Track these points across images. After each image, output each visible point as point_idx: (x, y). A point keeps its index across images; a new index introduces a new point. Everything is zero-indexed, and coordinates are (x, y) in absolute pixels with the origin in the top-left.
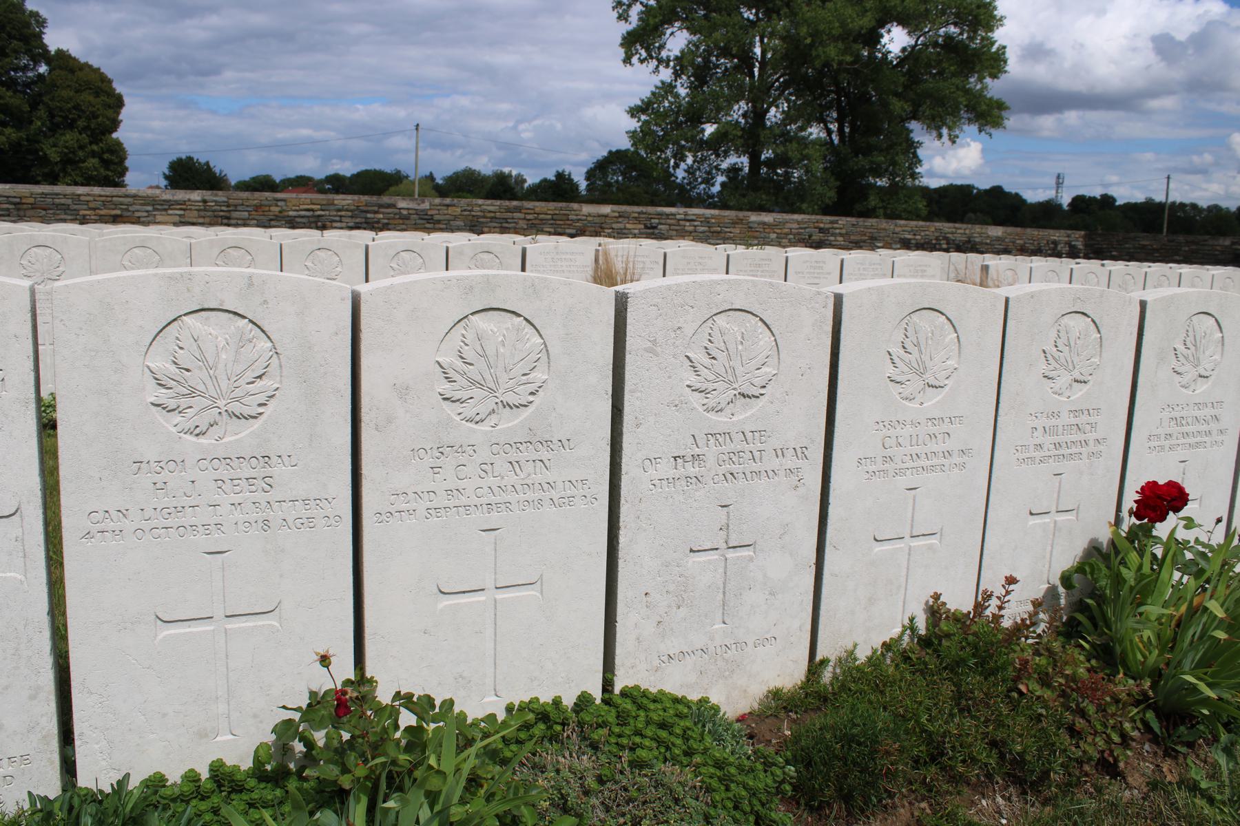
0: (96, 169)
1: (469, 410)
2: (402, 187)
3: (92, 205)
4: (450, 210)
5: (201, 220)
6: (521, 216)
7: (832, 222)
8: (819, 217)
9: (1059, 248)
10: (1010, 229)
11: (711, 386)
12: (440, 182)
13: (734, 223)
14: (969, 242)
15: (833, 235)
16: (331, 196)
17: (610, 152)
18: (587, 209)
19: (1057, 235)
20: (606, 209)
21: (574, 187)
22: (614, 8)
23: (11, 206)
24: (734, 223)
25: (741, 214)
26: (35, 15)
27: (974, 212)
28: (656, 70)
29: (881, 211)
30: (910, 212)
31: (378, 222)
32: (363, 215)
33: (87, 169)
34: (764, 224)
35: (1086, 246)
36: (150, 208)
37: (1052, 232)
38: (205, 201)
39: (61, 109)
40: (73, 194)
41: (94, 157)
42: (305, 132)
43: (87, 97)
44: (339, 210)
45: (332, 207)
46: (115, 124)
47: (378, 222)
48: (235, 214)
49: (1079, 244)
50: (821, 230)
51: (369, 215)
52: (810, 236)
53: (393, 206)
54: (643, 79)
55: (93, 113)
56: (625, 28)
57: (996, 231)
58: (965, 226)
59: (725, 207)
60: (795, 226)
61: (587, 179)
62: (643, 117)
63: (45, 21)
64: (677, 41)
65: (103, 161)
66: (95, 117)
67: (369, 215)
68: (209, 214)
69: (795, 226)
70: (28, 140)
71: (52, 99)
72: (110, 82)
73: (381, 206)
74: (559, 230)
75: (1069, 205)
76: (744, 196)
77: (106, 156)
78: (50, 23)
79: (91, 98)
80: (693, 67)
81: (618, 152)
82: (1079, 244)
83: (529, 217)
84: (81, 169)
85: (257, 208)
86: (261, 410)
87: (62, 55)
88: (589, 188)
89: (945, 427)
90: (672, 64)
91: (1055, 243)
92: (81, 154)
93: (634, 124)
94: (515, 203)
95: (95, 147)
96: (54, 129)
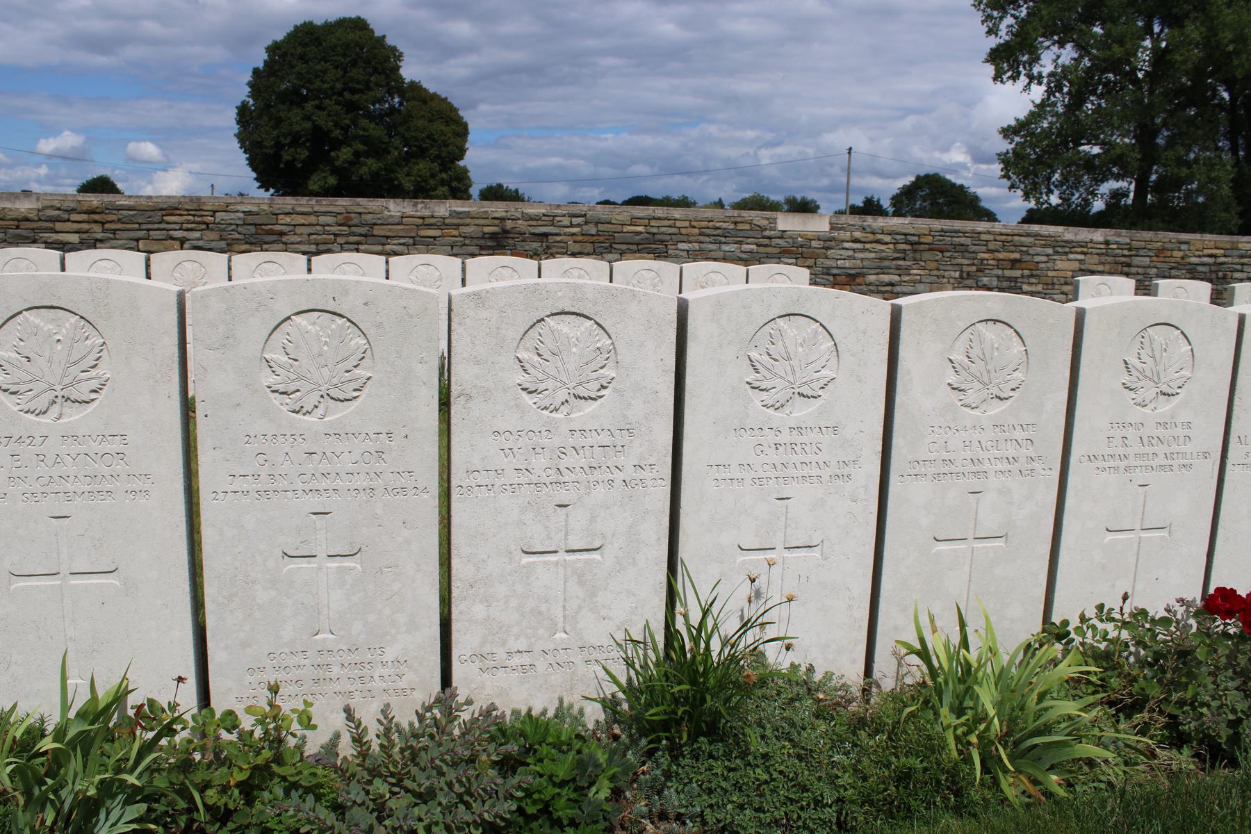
3: (992, 246)
5: (1100, 268)
16: (1235, 238)
17: (918, 178)
22: (983, 22)
23: (908, 247)
26: (394, 49)
28: (1027, 88)
36: (1050, 251)
38: (1107, 243)
39: (416, 139)
40: (974, 232)
41: (443, 185)
42: (554, 160)
43: (439, 126)
45: (1236, 253)
46: (461, 152)
48: (1136, 261)
54: (1014, 100)
55: (444, 142)
56: (993, 42)
57: (395, 208)
62: (1017, 139)
63: (401, 55)
64: (1055, 57)
66: (446, 144)
68: (1110, 259)
70: (385, 169)
71: (408, 129)
72: (456, 110)
74: (322, 247)
77: (454, 184)
78: (405, 58)
79: (443, 128)
80: (1076, 85)
81: (927, 176)
85: (1160, 252)
86: (93, 396)
87: (415, 87)
90: (1045, 80)
92: (432, 182)
93: (1005, 146)
95: (444, 176)
96: (408, 157)
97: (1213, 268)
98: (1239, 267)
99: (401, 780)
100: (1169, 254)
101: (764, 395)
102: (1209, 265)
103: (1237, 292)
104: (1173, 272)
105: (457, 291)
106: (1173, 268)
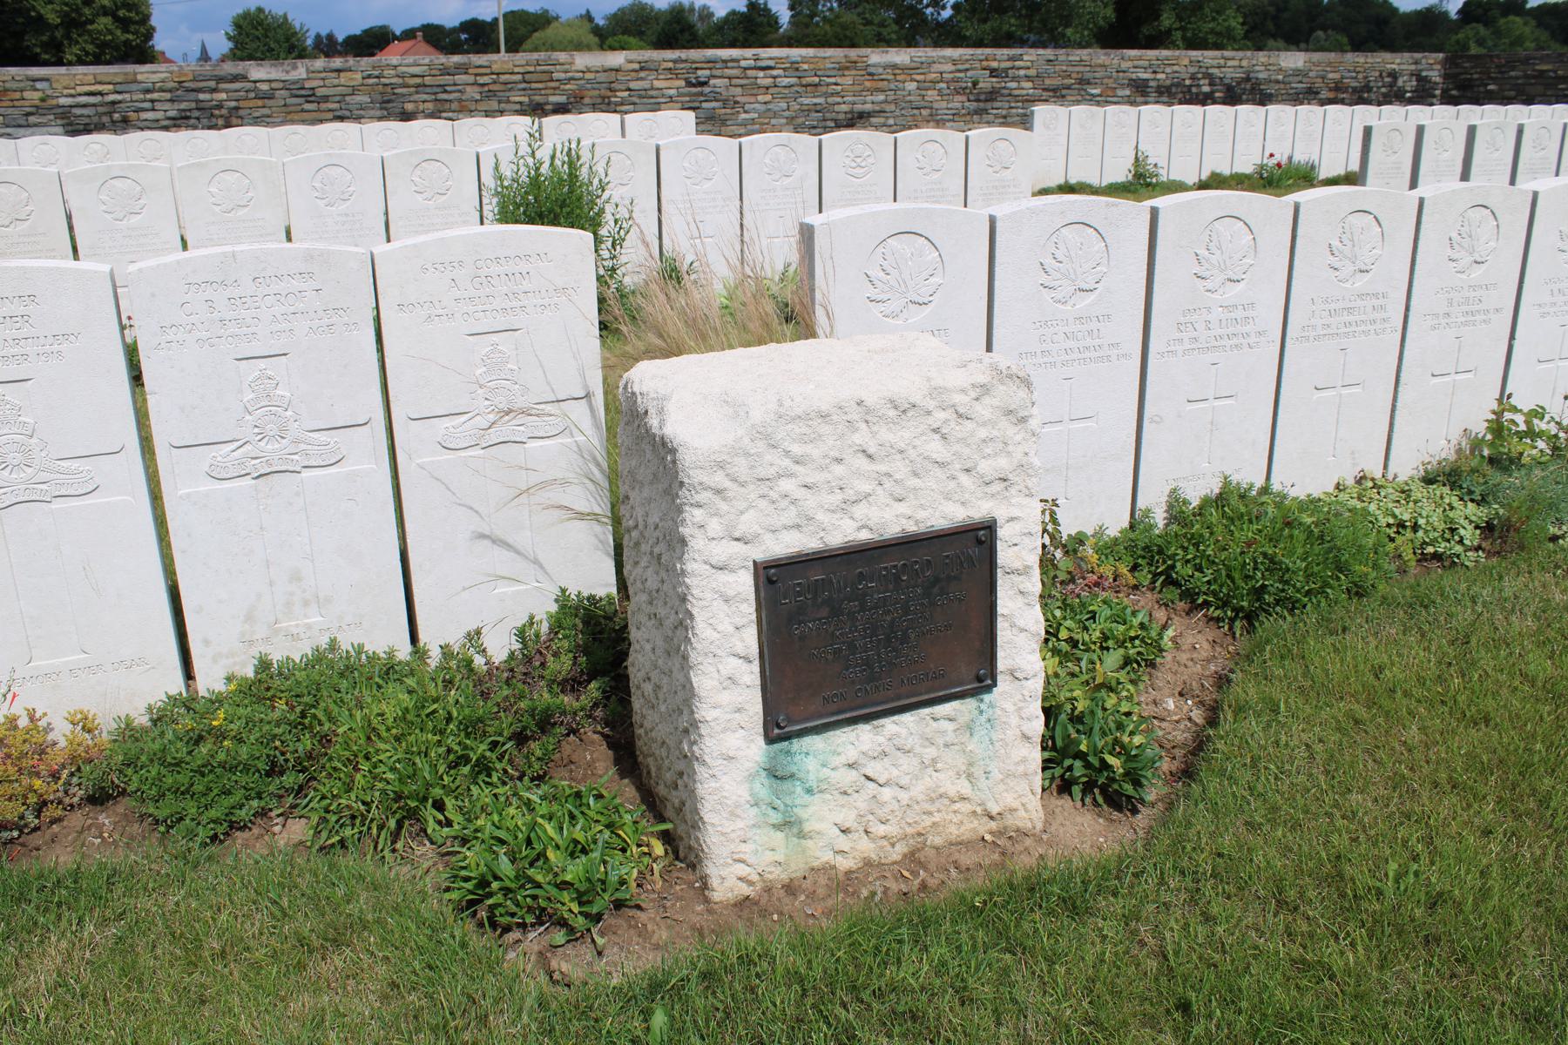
0: (110, 32)
1: (1058, 295)
2: (549, 32)
4: (344, 78)
6: (471, 79)
7: (1012, 59)
8: (988, 51)
9: (1400, 83)
10: (1317, 56)
11: (1057, 283)
12: (601, 23)
13: (842, 69)
14: (1248, 79)
15: (1014, 79)
18: (582, 60)
19: (1399, 62)
20: (617, 59)
21: (773, 21)
24: (842, 69)
25: (853, 53)
27: (1324, 29)
29: (1179, 34)
30: (1219, 34)
31: (220, 107)
32: (193, 96)
33: (99, 32)
34: (895, 66)
35: (1446, 77)
37: (1388, 56)
41: (105, 14)
44: (148, 91)
45: (134, 87)
47: (220, 107)
49: (1435, 75)
50: (993, 72)
51: (202, 96)
52: (975, 84)
53: (244, 78)
57: (1293, 60)
58: (1240, 54)
59: (958, 40)
60: (949, 67)
61: (792, 8)
65: (116, 18)
67: (202, 96)
69: (949, 67)
73: (220, 79)
75: (1459, 12)
76: (985, 21)
77: (121, 13)
82: (1435, 75)
83: (481, 80)
84: (89, 33)
88: (794, 21)
89: (1094, 325)
91: (1394, 75)
92: (87, 11)
94: (456, 59)
97: (101, 109)
98: (147, 105)
99: (21, 832)
100: (18, 95)
101: (881, 307)
102: (94, 105)
103: (1036, 116)
104: (32, 119)
105: (381, 248)
106: (28, 114)
